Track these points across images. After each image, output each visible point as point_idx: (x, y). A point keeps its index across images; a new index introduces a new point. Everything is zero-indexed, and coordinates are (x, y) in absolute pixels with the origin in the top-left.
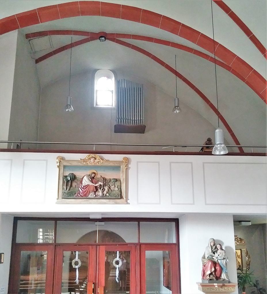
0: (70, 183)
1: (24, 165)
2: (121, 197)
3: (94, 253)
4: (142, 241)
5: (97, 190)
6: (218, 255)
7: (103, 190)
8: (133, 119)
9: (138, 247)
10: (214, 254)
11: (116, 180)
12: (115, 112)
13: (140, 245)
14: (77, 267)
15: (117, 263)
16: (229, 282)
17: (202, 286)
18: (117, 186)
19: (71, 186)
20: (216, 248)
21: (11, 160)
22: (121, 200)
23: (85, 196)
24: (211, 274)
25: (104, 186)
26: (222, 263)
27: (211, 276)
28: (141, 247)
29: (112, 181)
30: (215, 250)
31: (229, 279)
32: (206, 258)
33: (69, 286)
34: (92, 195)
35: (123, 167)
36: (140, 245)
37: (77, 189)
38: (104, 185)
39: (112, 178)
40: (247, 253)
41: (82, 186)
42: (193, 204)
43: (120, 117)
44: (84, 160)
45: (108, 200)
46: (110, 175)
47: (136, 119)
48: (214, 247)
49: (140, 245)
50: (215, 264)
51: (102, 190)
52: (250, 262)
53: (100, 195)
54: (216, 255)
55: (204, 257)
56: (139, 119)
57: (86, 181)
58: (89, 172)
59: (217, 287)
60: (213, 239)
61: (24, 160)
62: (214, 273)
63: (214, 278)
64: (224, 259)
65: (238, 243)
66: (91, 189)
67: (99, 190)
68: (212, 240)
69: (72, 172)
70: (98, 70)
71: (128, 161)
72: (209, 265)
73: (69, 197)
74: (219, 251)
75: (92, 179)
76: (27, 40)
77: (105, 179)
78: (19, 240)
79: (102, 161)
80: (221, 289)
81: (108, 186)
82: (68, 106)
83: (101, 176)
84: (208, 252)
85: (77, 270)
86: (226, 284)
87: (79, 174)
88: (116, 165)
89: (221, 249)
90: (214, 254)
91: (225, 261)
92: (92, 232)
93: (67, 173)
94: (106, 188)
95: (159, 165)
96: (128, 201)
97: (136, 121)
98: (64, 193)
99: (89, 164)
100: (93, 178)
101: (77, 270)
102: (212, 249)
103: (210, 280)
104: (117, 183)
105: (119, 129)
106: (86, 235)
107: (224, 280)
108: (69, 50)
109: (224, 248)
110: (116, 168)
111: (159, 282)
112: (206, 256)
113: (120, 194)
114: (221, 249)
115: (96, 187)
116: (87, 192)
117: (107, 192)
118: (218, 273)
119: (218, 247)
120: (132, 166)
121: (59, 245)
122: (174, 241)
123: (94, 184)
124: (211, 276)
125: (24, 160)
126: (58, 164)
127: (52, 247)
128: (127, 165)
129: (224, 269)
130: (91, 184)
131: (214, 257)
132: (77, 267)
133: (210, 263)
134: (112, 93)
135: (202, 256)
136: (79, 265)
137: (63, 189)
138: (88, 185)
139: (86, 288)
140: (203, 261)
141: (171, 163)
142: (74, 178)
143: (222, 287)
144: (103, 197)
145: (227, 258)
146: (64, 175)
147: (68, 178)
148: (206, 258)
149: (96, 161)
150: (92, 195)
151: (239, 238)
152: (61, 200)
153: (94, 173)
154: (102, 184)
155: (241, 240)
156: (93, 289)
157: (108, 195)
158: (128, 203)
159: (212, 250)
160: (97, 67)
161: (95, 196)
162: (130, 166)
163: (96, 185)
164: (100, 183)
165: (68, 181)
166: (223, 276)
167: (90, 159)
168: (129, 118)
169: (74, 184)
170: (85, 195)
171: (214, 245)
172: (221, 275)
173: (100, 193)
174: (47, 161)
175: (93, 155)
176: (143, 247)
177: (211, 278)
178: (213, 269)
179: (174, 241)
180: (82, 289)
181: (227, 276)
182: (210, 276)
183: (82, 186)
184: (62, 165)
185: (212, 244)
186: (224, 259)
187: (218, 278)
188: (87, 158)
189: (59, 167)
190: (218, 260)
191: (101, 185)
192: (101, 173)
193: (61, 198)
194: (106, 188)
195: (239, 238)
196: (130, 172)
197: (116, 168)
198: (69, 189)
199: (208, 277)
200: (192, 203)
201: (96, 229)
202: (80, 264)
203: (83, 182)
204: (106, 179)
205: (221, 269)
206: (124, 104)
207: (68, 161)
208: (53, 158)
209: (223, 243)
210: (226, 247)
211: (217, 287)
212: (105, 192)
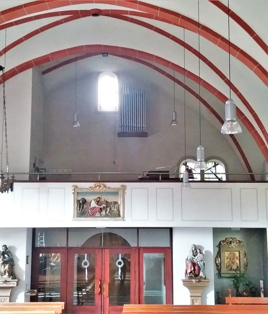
1: (48, 193)
2: (119, 216)
3: (100, 255)
5: (101, 211)
6: (198, 258)
9: (137, 250)
11: (116, 203)
12: (118, 116)
13: (139, 248)
14: (86, 267)
15: (85, 264)
17: (183, 281)
19: (83, 207)
23: (93, 215)
24: (191, 272)
25: (106, 208)
26: (201, 264)
27: (191, 274)
28: (140, 250)
30: (196, 254)
31: (206, 277)
32: (189, 260)
33: (77, 285)
34: (98, 214)
35: (121, 193)
36: (139, 249)
37: (87, 210)
38: (106, 207)
40: (245, 254)
43: (123, 124)
45: (109, 218)
46: (110, 199)
47: (138, 126)
49: (139, 249)
50: (194, 264)
51: (105, 210)
53: (104, 215)
54: (196, 257)
55: (187, 260)
56: (141, 126)
57: (93, 204)
58: (96, 197)
59: (194, 282)
60: (195, 245)
63: (193, 275)
64: (201, 261)
67: (103, 210)
70: (102, 72)
71: (124, 188)
72: (190, 266)
73: (81, 216)
74: (199, 254)
75: (98, 202)
77: (107, 202)
79: (105, 188)
80: (198, 284)
81: (110, 207)
82: (74, 123)
84: (190, 255)
85: (86, 270)
86: (201, 280)
87: (88, 198)
89: (201, 253)
90: (195, 257)
93: (80, 198)
94: (108, 209)
96: (125, 219)
97: (138, 128)
98: (78, 213)
99: (96, 191)
101: (86, 270)
103: (190, 277)
104: (116, 206)
105: (121, 135)
107: (201, 277)
113: (118, 213)
115: (101, 208)
116: (94, 213)
117: (109, 212)
118: (197, 272)
119: (198, 251)
121: (72, 248)
123: (99, 206)
126: (73, 191)
127: (65, 251)
129: (202, 269)
130: (97, 206)
131: (194, 260)
132: (86, 267)
133: (191, 264)
134: (116, 93)
136: (87, 265)
137: (77, 210)
138: (95, 207)
140: (186, 262)
142: (84, 201)
144: (106, 216)
145: (204, 260)
146: (78, 199)
147: (80, 202)
149: (101, 188)
150: (98, 214)
152: (75, 218)
153: (99, 198)
154: (105, 206)
155: (240, 242)
156: (100, 285)
157: (109, 214)
158: (124, 220)
159: (193, 253)
160: (98, 70)
161: (100, 215)
163: (101, 207)
164: (104, 205)
165: (80, 204)
166: (201, 274)
167: (96, 187)
168: (132, 126)
169: (85, 206)
170: (93, 215)
172: (199, 273)
173: (103, 213)
174: (64, 188)
175: (98, 184)
176: (141, 250)
177: (190, 276)
178: (193, 269)
180: (89, 290)
181: (204, 273)
182: (190, 274)
184: (77, 192)
185: (193, 249)
186: (201, 261)
187: (196, 276)
188: (94, 186)
189: (73, 193)
190: (197, 262)
191: (104, 207)
192: (104, 198)
194: (108, 209)
196: (126, 196)
197: (115, 193)
198: (82, 210)
201: (101, 232)
203: (92, 205)
207: (80, 189)
208: (69, 187)
209: (203, 248)
210: (206, 252)
211: (194, 282)
212: (107, 212)
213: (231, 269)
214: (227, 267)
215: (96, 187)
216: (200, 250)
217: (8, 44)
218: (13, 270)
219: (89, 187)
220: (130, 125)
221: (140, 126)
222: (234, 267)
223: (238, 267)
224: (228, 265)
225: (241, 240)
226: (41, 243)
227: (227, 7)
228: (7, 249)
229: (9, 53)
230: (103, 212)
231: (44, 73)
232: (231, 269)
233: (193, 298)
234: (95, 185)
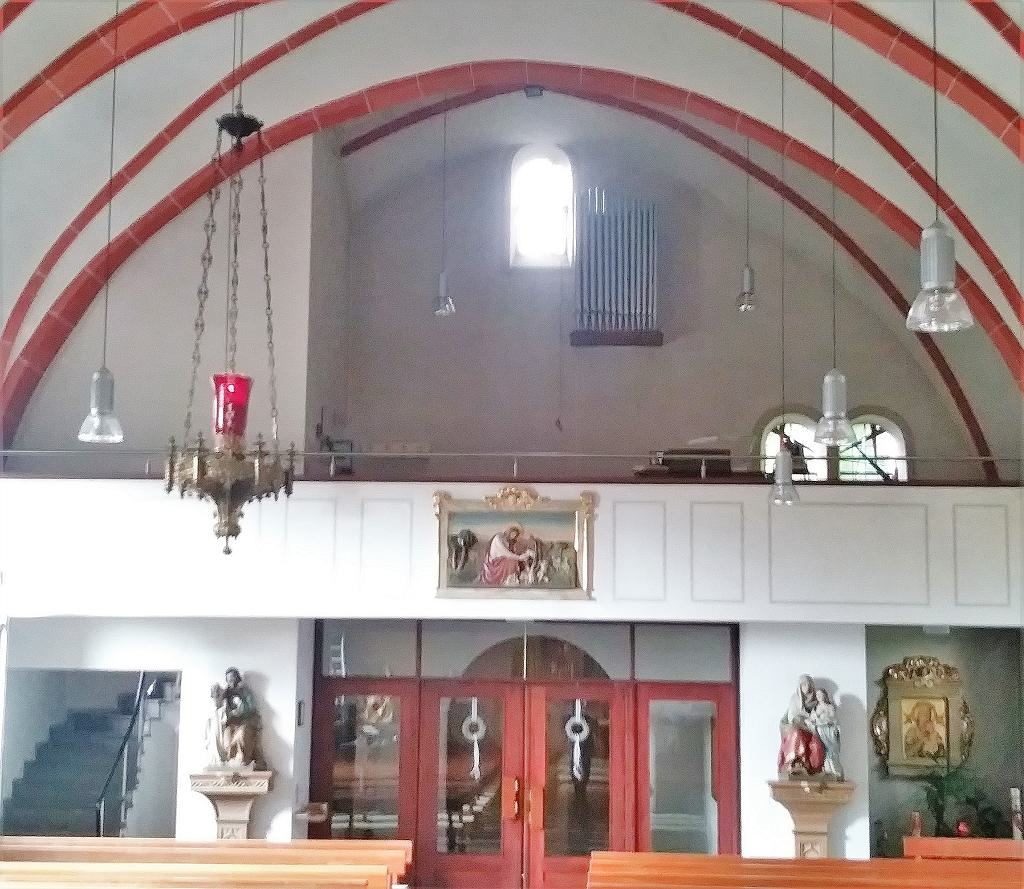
0: (463, 552)
1: (362, 513)
2: (577, 585)
5: (522, 569)
7: (537, 570)
8: (626, 312)
10: (809, 712)
16: (841, 780)
18: (566, 559)
19: (466, 558)
20: (814, 698)
22: (576, 592)
23: (496, 582)
24: (798, 759)
26: (827, 734)
28: (638, 691)
29: (556, 547)
39: (555, 540)
40: (966, 709)
41: (491, 560)
42: (743, 600)
43: (586, 305)
44: (493, 499)
46: (550, 534)
47: (633, 312)
48: (810, 697)
50: (806, 736)
52: (972, 735)
54: (814, 715)
55: (785, 721)
56: (644, 312)
57: (498, 549)
58: (505, 527)
62: (804, 759)
64: (830, 725)
65: (938, 681)
66: (511, 567)
68: (805, 679)
69: (467, 528)
71: (592, 500)
74: (822, 706)
75: (512, 543)
77: (539, 544)
82: (438, 302)
83: (532, 537)
86: (830, 785)
87: (481, 531)
88: (566, 509)
89: (827, 701)
90: (809, 712)
91: (832, 730)
93: (457, 530)
94: (543, 566)
96: (593, 594)
97: (633, 320)
98: (451, 577)
99: (504, 509)
100: (514, 541)
102: (804, 700)
104: (567, 555)
108: (439, 119)
109: (837, 702)
110: (565, 517)
111: (701, 786)
114: (827, 701)
118: (814, 759)
120: (603, 512)
128: (591, 512)
129: (831, 749)
130: (509, 555)
131: (806, 721)
133: (796, 734)
135: (782, 716)
137: (449, 565)
138: (503, 559)
139: (496, 803)
141: (692, 504)
142: (471, 541)
143: (821, 789)
144: (537, 584)
148: (790, 720)
151: (942, 663)
152: (444, 590)
155: (948, 670)
156: (517, 794)
157: (547, 579)
158: (591, 598)
162: (596, 511)
165: (458, 550)
166: (829, 766)
167: (505, 497)
168: (614, 310)
169: (472, 555)
171: (810, 692)
172: (822, 764)
173: (529, 576)
176: (642, 692)
178: (802, 750)
181: (838, 765)
182: (793, 765)
183: (491, 560)
184: (449, 513)
185: (805, 690)
187: (814, 770)
191: (530, 558)
192: (531, 530)
193: (445, 586)
194: (543, 566)
195: (942, 663)
196: (597, 524)
199: (790, 768)
202: (482, 730)
204: (542, 544)
205: (823, 749)
206: (593, 290)
207: (459, 502)
208: (424, 494)
209: (835, 687)
210: (844, 698)
212: (540, 575)
215: (505, 497)
222: (931, 747)
223: (940, 746)
225: (951, 664)
233: (804, 838)
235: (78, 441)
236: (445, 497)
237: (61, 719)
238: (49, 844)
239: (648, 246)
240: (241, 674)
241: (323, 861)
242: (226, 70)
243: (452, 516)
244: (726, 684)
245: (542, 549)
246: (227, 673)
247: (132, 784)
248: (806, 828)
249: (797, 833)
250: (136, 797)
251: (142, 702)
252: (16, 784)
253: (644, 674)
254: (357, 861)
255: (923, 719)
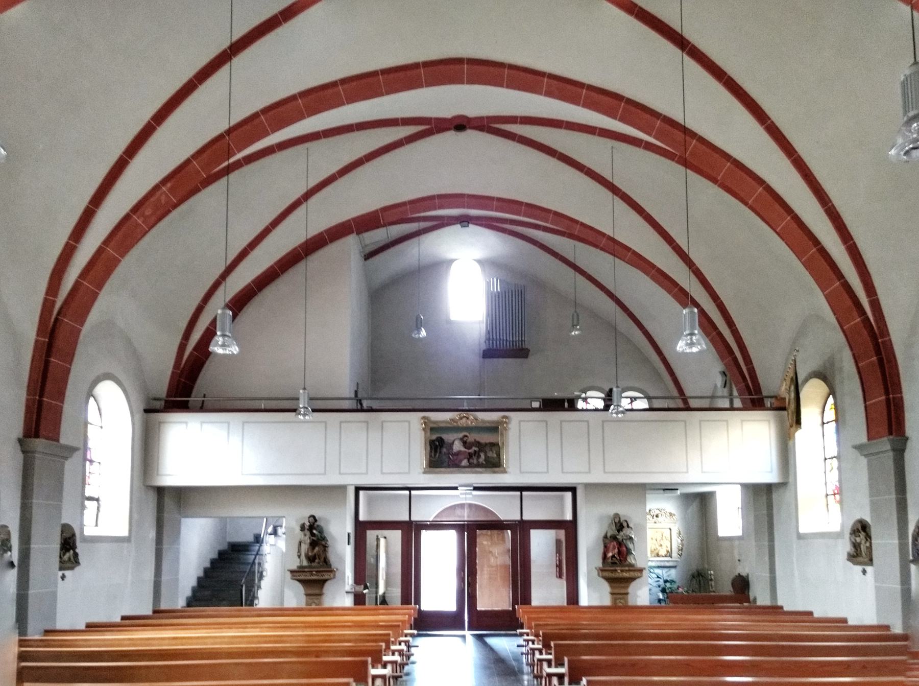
4: (526, 517)
7: (479, 456)
17: (331, 571)
21: (367, 422)
44: (453, 420)
46: (485, 438)
47: (514, 339)
57: (458, 446)
58: (461, 435)
61: (382, 422)
67: (474, 457)
69: (439, 435)
75: (465, 443)
76: (527, 345)
78: (362, 518)
87: (448, 437)
88: (493, 425)
92: (458, 505)
93: (434, 437)
95: (547, 424)
106: (447, 509)
110: (494, 428)
112: (609, 535)
115: (469, 453)
122: (569, 517)
124: (613, 559)
125: (382, 422)
142: (441, 440)
144: (479, 465)
154: (476, 449)
155: (671, 514)
163: (470, 451)
167: (461, 418)
177: (612, 561)
179: (569, 517)
182: (612, 559)
200: (587, 470)
208: (415, 419)
213: (658, 555)
214: (652, 552)
215: (461, 418)
216: (626, 521)
217: (313, 183)
218: (327, 555)
219: (450, 420)
220: (501, 337)
221: (517, 339)
222: (663, 552)
223: (668, 552)
224: (653, 549)
225: (673, 512)
226: (693, 48)
227: (681, 125)
228: (316, 520)
229: (313, 200)
230: (473, 459)
231: (369, 256)
232: (658, 555)
233: (615, 596)
234: (460, 415)
235: (370, 656)
236: (426, 421)
237: (224, 547)
238: (203, 611)
239: (512, 329)
240: (317, 518)
241: (216, 633)
242: (302, 190)
243: (432, 429)
244: (569, 521)
245: (481, 447)
246: (309, 518)
247: (261, 577)
248: (616, 591)
249: (612, 594)
250: (264, 583)
251: (265, 536)
252: (199, 580)
253: (530, 515)
254: (195, 633)
255: (659, 539)
